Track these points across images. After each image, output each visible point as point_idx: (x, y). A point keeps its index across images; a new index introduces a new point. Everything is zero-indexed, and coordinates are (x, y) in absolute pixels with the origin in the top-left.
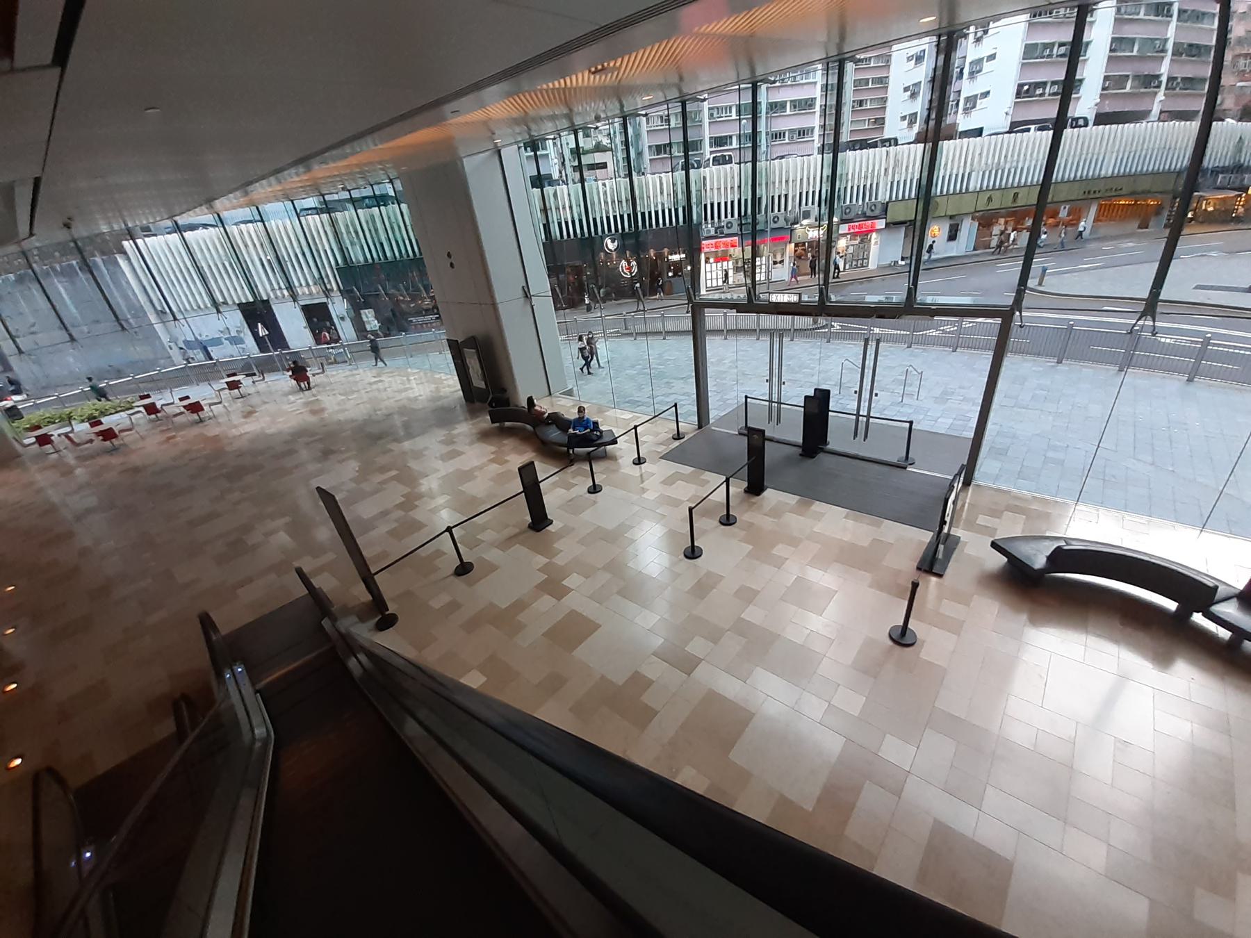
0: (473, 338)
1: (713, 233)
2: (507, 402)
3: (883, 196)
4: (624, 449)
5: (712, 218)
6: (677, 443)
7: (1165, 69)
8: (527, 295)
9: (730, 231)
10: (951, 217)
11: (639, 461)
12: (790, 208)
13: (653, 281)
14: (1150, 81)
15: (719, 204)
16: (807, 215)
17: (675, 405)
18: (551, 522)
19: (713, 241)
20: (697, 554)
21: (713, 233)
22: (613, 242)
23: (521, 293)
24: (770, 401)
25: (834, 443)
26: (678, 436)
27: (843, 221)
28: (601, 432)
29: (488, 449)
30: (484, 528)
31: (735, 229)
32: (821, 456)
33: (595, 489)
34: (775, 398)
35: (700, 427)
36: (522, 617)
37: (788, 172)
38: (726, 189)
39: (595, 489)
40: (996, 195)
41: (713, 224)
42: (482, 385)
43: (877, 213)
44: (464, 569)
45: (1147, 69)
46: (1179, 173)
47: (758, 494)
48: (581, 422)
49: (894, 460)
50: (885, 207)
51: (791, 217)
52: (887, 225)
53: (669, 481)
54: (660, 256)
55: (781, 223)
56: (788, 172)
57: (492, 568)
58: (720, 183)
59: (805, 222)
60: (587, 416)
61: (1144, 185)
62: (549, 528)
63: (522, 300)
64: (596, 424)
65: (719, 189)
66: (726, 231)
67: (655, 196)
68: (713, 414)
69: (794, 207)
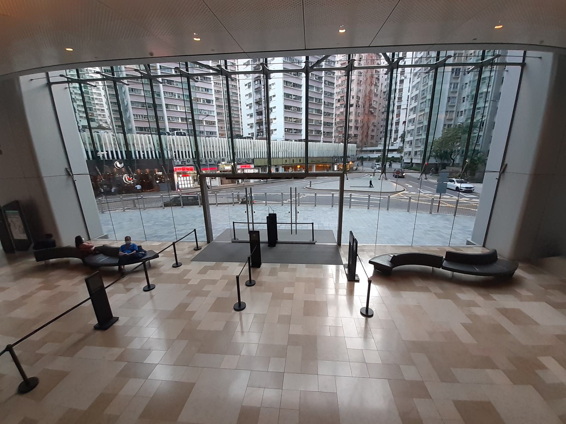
0: (17, 202)
1: (180, 163)
2: (53, 244)
3: (251, 156)
4: (164, 262)
5: (179, 157)
6: (197, 253)
7: (322, 129)
8: (69, 173)
9: (189, 164)
10: (275, 166)
11: (177, 265)
12: (216, 157)
13: (148, 185)
14: (319, 132)
15: (182, 152)
16: (223, 160)
17: (195, 230)
18: (117, 319)
19: (181, 167)
20: (242, 307)
21: (180, 163)
22: (120, 163)
23: (64, 173)
24: (248, 223)
25: (280, 238)
26: (197, 248)
27: (238, 164)
28: (145, 252)
29: (35, 282)
30: (43, 342)
31: (191, 163)
32: (277, 245)
33: (149, 288)
34: (250, 221)
35: (208, 242)
36: (111, 410)
37: (213, 142)
38: (185, 146)
39: (149, 288)
40: (288, 160)
41: (180, 160)
42: (24, 237)
43: (251, 162)
44: (28, 386)
45: (318, 129)
46: (122, 283)
47: (260, 267)
48: (128, 246)
49: (308, 241)
50: (253, 160)
51: (217, 160)
52: (255, 167)
53: (203, 271)
54: (152, 172)
55: (213, 162)
56: (213, 142)
57: (62, 375)
58: (178, 144)
59: (223, 163)
60: (132, 242)
61: (325, 160)
62: (117, 324)
63: (65, 177)
64: (140, 247)
65: (181, 145)
66: (187, 163)
67: (146, 144)
68: (215, 235)
69: (217, 157)
